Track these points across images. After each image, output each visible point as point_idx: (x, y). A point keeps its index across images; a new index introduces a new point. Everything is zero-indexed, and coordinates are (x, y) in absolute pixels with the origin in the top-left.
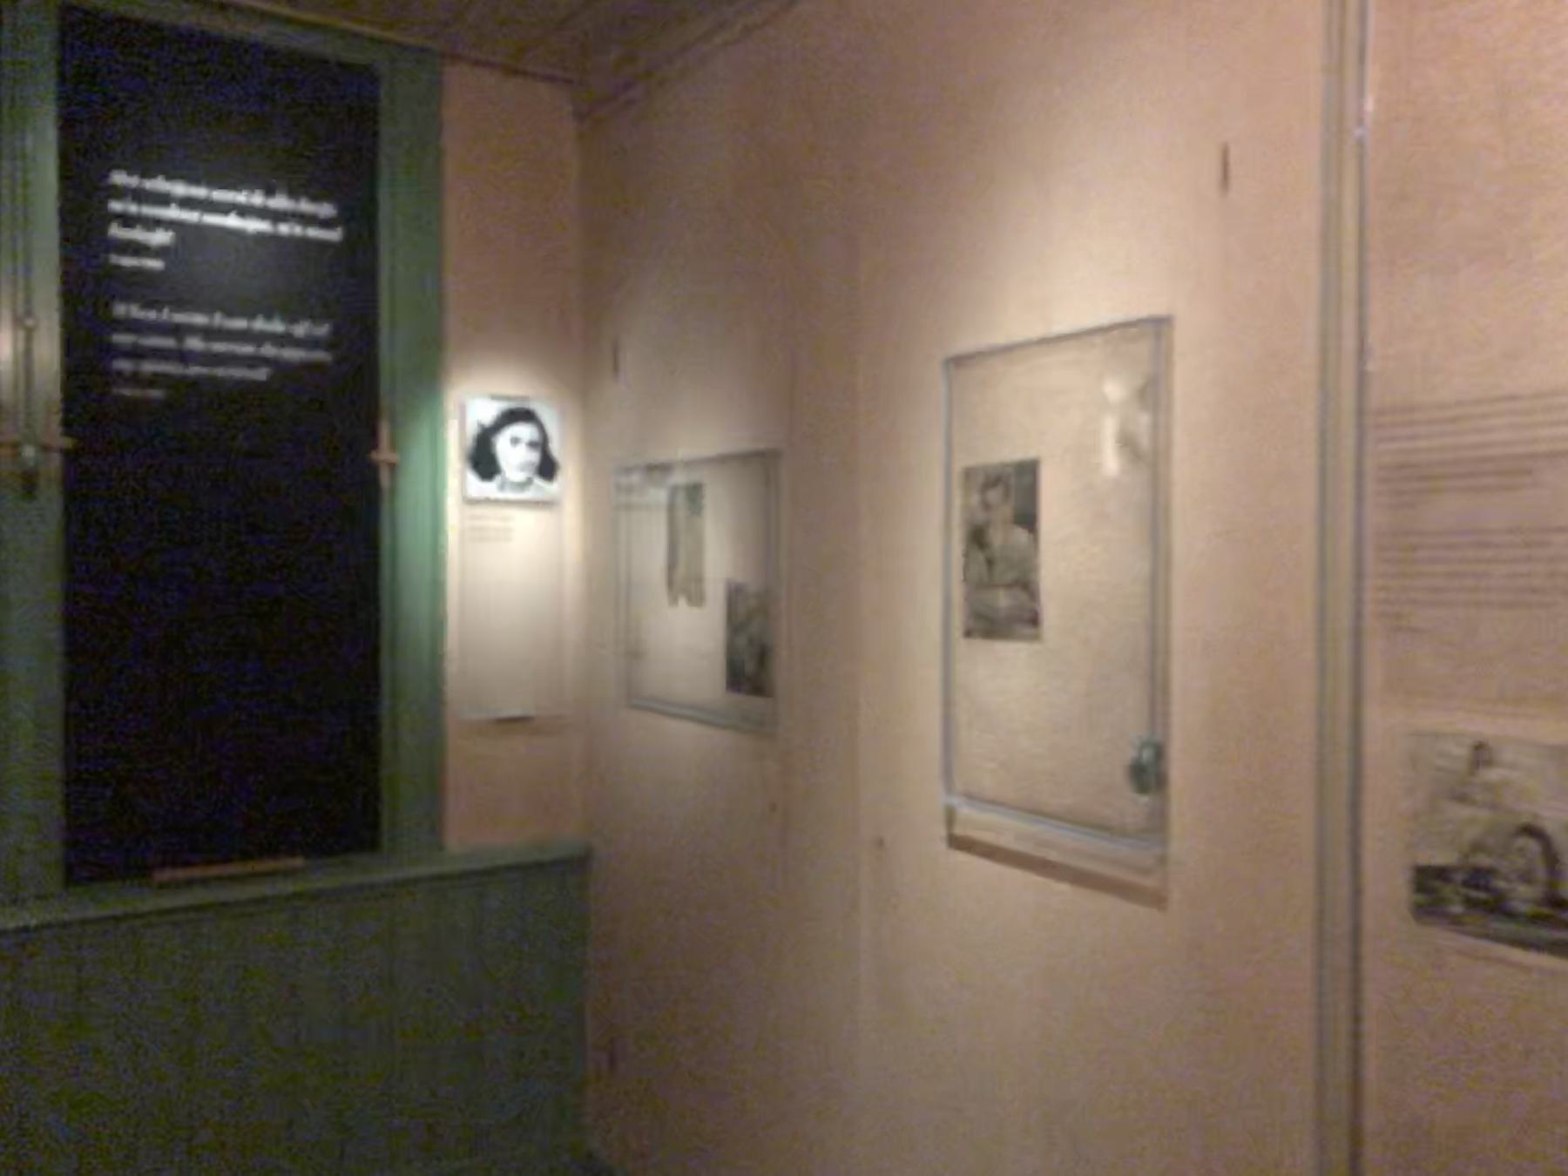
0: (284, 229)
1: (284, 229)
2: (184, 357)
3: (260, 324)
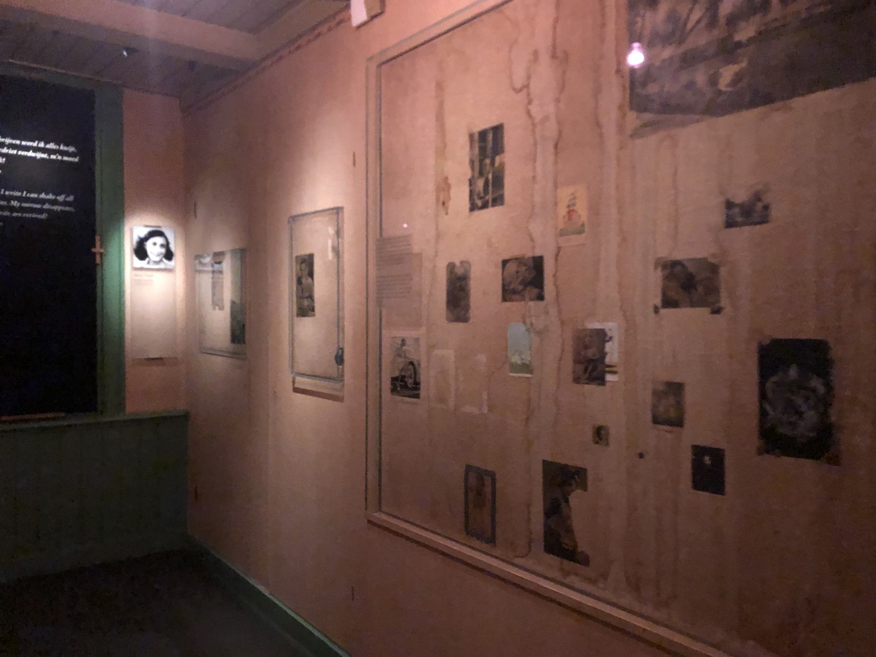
0: (53, 157)
1: (53, 157)
2: (12, 209)
3: (43, 196)
